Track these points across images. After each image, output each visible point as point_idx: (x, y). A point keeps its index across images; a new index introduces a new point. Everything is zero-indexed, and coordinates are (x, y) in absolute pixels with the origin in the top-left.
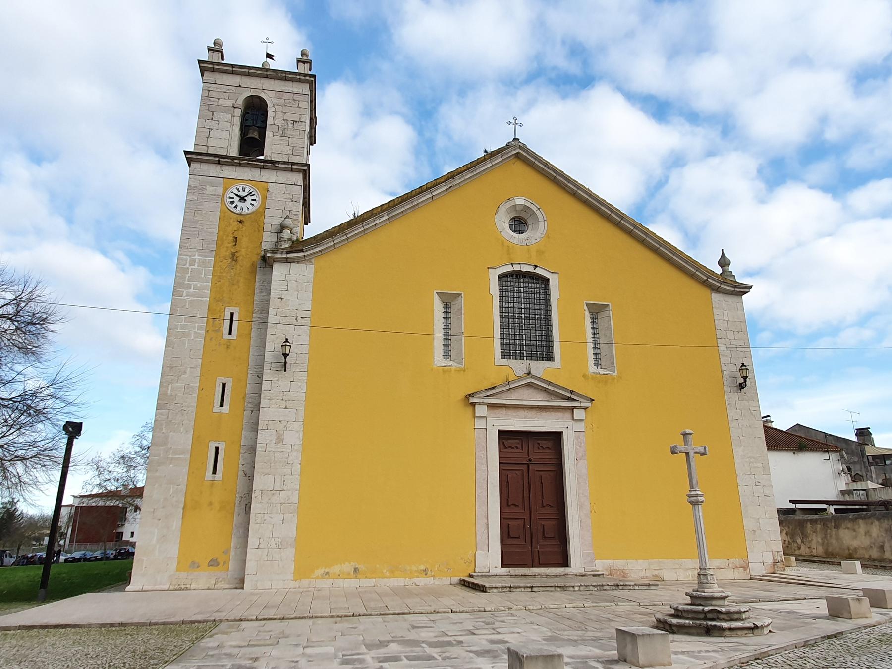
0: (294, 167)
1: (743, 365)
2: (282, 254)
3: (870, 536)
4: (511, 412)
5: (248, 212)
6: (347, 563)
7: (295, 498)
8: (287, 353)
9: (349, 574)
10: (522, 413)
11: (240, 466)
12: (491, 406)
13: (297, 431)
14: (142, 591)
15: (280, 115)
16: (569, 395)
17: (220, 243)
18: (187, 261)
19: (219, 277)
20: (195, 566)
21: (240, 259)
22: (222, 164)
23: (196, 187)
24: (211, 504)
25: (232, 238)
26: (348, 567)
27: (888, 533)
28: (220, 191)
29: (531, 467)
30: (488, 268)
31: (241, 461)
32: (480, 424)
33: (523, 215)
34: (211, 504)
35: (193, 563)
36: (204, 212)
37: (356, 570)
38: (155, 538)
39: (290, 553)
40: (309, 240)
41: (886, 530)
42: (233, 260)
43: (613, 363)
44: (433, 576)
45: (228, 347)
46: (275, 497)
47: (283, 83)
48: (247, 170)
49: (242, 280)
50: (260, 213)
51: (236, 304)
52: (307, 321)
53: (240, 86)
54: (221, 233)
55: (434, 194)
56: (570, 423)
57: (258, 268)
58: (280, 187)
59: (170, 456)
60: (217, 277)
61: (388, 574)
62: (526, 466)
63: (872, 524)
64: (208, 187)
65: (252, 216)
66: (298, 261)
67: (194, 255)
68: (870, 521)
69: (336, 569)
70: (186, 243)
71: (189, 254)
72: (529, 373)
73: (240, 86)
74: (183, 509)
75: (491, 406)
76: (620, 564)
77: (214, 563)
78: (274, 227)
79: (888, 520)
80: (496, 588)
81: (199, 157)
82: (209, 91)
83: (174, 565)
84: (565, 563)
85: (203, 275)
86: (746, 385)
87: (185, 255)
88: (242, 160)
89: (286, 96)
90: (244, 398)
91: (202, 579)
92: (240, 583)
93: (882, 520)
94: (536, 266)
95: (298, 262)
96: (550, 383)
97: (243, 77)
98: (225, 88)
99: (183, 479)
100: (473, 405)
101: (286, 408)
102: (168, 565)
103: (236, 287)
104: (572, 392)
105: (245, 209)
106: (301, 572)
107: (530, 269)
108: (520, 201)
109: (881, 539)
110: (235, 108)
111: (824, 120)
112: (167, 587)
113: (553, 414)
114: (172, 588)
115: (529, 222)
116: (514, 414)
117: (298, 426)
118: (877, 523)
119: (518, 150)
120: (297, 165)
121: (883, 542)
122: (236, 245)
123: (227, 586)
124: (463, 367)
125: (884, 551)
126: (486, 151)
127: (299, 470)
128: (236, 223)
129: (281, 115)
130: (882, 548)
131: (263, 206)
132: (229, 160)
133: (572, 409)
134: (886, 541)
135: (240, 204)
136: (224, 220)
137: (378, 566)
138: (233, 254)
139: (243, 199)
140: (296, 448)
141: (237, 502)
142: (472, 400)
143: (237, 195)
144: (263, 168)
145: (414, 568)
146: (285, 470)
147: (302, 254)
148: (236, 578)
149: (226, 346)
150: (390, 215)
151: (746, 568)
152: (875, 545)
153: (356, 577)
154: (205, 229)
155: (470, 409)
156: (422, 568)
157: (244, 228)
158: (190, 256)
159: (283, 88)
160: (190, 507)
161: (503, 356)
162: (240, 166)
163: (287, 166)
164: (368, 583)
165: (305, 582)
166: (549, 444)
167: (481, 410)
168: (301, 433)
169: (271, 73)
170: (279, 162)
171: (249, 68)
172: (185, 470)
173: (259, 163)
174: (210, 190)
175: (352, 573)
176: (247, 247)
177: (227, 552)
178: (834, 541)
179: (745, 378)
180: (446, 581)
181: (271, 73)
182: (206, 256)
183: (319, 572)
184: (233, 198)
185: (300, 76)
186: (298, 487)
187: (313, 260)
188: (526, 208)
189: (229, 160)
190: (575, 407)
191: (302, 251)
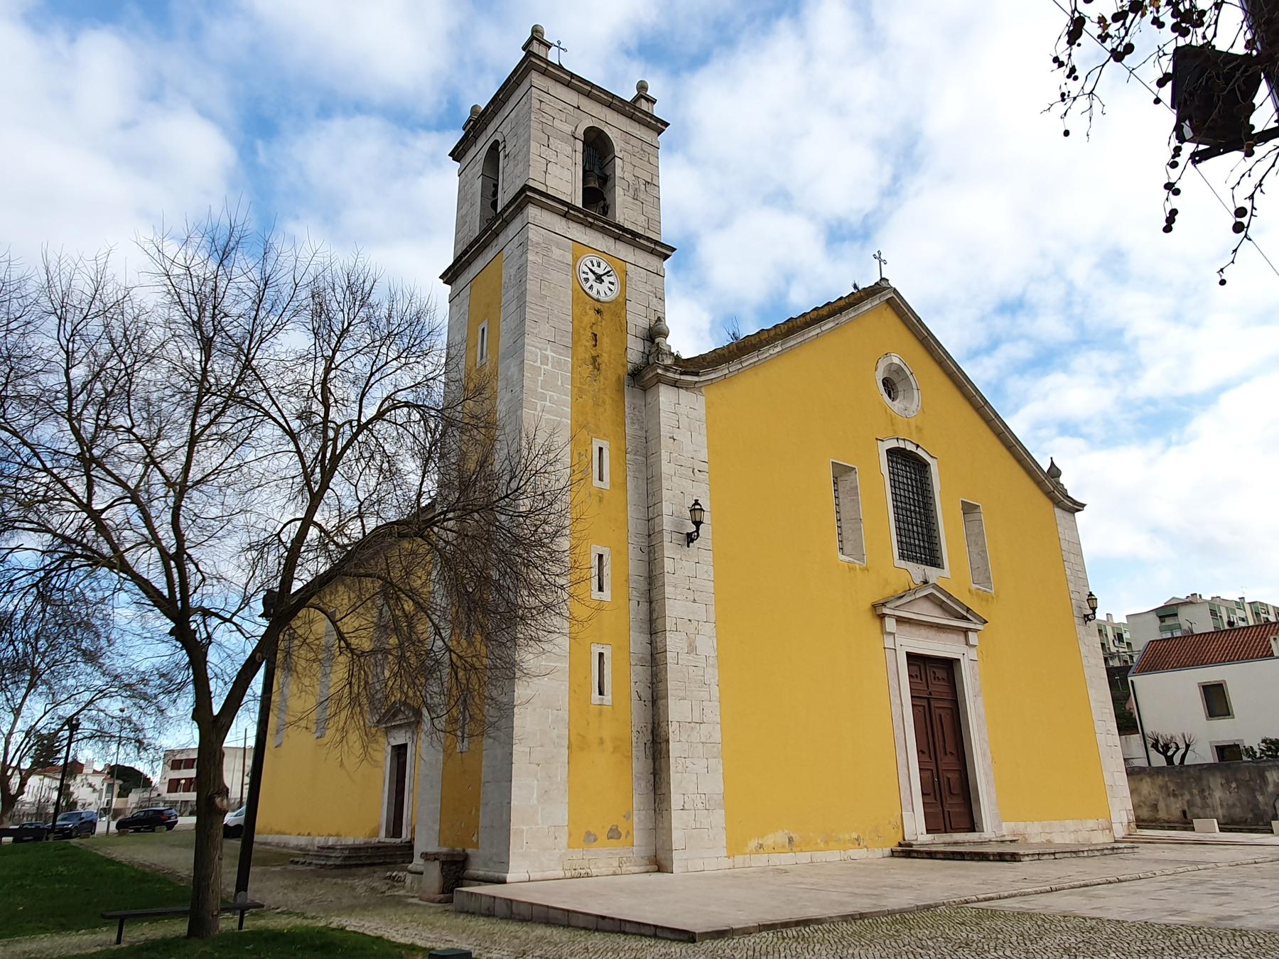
0: (658, 248)
1: (697, 502)
2: (675, 373)
3: (1140, 794)
4: (914, 630)
5: (607, 299)
6: (780, 831)
7: (717, 736)
8: (698, 519)
9: (784, 846)
10: (924, 632)
11: (633, 684)
12: (900, 620)
13: (710, 637)
14: (529, 881)
15: (628, 167)
16: (965, 614)
17: (576, 333)
18: (537, 356)
19: (580, 390)
20: (590, 838)
21: (603, 367)
22: (568, 219)
23: (538, 244)
24: (602, 741)
25: (590, 334)
26: (780, 837)
27: (1164, 790)
28: (569, 258)
29: (933, 703)
30: (877, 439)
31: (634, 678)
32: (889, 642)
33: (895, 378)
34: (602, 741)
35: (588, 834)
36: (552, 285)
37: (790, 840)
38: (535, 796)
39: (719, 817)
40: (696, 360)
41: (1161, 788)
42: (595, 367)
43: (989, 578)
44: (866, 847)
45: (600, 501)
46: (695, 733)
47: (627, 121)
48: (598, 235)
49: (608, 401)
50: (620, 304)
51: (604, 435)
52: (704, 476)
53: (578, 108)
54: (575, 322)
55: (823, 329)
56: (965, 649)
57: (626, 387)
58: (640, 273)
59: (543, 663)
60: (578, 392)
61: (822, 845)
62: (926, 700)
63: (1141, 780)
64: (553, 248)
65: (612, 306)
66: (687, 387)
67: (546, 350)
68: (1139, 777)
69: (769, 840)
70: (535, 329)
71: (540, 346)
72: (926, 582)
73: (578, 108)
74: (568, 748)
75: (900, 620)
76: (1020, 826)
77: (614, 834)
78: (639, 329)
79: (1164, 776)
80: (1028, 855)
81: (543, 199)
82: (541, 101)
83: (564, 839)
84: (972, 826)
85: (559, 383)
86: (698, 535)
87: (533, 346)
88: (597, 219)
89: (633, 141)
90: (627, 581)
91: (603, 860)
92: (659, 864)
93: (1155, 777)
94: (918, 446)
95: (687, 389)
96: (950, 596)
97: (581, 96)
98: (561, 105)
99: (563, 700)
100: (882, 617)
101: (694, 601)
102: (556, 838)
103: (601, 410)
104: (968, 610)
105: (602, 294)
106: (734, 848)
107: (911, 447)
108: (896, 360)
109: (1153, 796)
110: (576, 138)
111: (789, 277)
112: (561, 874)
113: (943, 635)
114: (568, 875)
115: (900, 387)
116: (917, 633)
117: (709, 629)
118: (1149, 780)
119: (892, 295)
120: (662, 247)
121: (1157, 800)
122: (595, 345)
123: (637, 869)
124: (865, 565)
125: (1158, 811)
126: (855, 287)
127: (718, 695)
128: (592, 312)
129: (631, 167)
130: (1155, 807)
131: (623, 296)
132: (581, 216)
133: (966, 631)
134: (1161, 799)
135: (596, 286)
136: (578, 304)
137: (811, 834)
138: (594, 359)
139: (599, 278)
140: (711, 661)
141: (634, 739)
142: (886, 611)
143: (591, 270)
144: (618, 239)
145: (847, 837)
146: (702, 693)
147: (696, 379)
148: (642, 858)
149: (598, 498)
150: (784, 347)
151: (1110, 829)
152: (1145, 804)
153: (792, 851)
154: (556, 312)
155: (877, 623)
156: (855, 835)
157: (604, 322)
158: (540, 349)
159: (629, 130)
160: (577, 746)
161: (902, 556)
162: (590, 227)
163: (649, 244)
164: (804, 857)
165: (739, 859)
166: (941, 673)
167: (890, 624)
168: (715, 641)
169: (617, 103)
170: (641, 236)
171: (593, 86)
172: (565, 687)
173: (617, 231)
174: (556, 253)
175: (787, 844)
176: (610, 351)
177: (628, 817)
178: (1244, 796)
179: (698, 524)
180: (878, 853)
181: (617, 103)
182: (560, 354)
183: (753, 844)
184: (587, 274)
185: (650, 118)
186: (719, 720)
187: (703, 390)
188: (899, 370)
189: (581, 216)
190: (970, 629)
191: (697, 374)
